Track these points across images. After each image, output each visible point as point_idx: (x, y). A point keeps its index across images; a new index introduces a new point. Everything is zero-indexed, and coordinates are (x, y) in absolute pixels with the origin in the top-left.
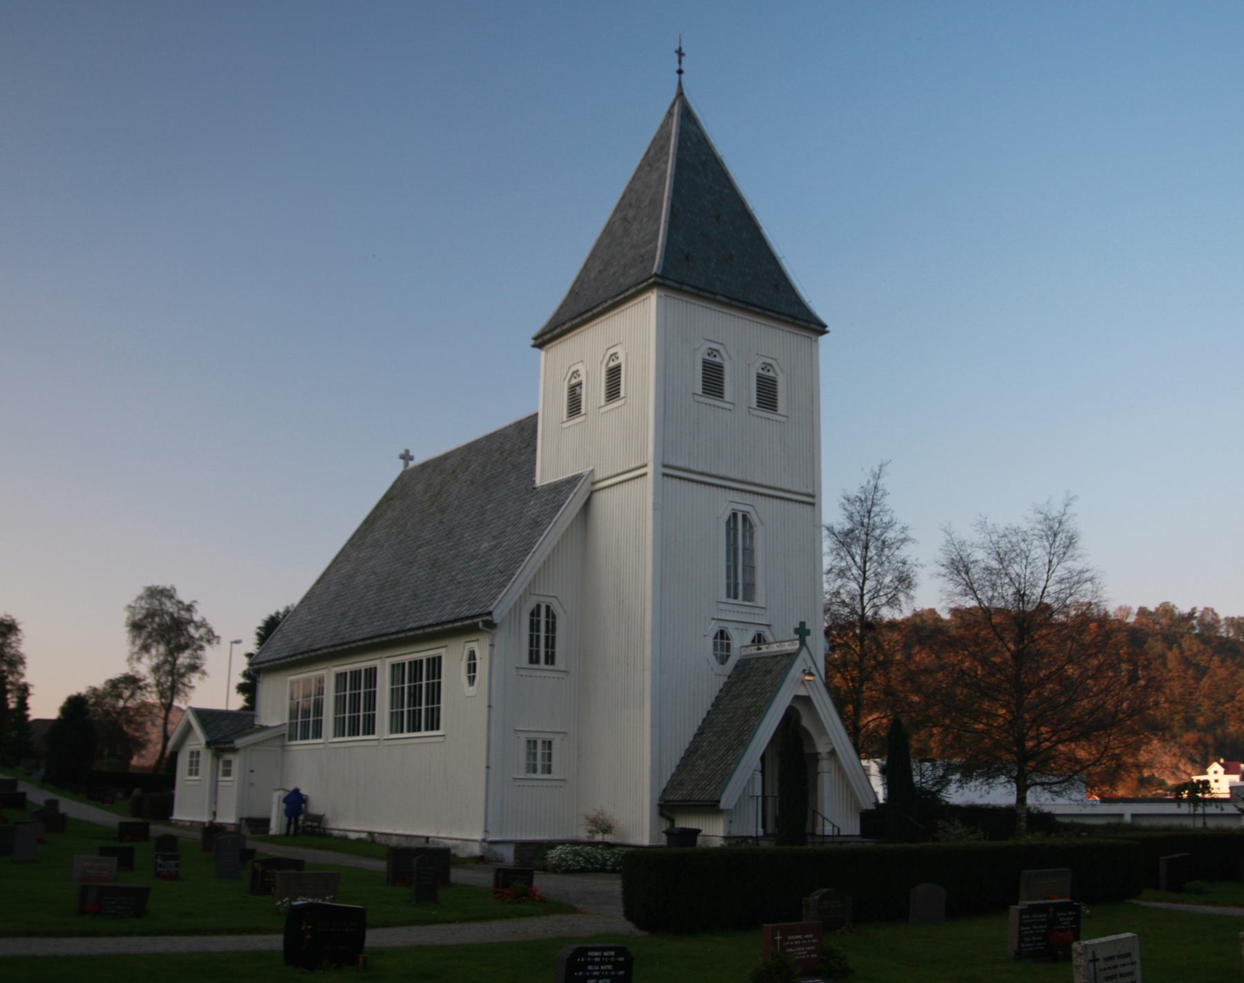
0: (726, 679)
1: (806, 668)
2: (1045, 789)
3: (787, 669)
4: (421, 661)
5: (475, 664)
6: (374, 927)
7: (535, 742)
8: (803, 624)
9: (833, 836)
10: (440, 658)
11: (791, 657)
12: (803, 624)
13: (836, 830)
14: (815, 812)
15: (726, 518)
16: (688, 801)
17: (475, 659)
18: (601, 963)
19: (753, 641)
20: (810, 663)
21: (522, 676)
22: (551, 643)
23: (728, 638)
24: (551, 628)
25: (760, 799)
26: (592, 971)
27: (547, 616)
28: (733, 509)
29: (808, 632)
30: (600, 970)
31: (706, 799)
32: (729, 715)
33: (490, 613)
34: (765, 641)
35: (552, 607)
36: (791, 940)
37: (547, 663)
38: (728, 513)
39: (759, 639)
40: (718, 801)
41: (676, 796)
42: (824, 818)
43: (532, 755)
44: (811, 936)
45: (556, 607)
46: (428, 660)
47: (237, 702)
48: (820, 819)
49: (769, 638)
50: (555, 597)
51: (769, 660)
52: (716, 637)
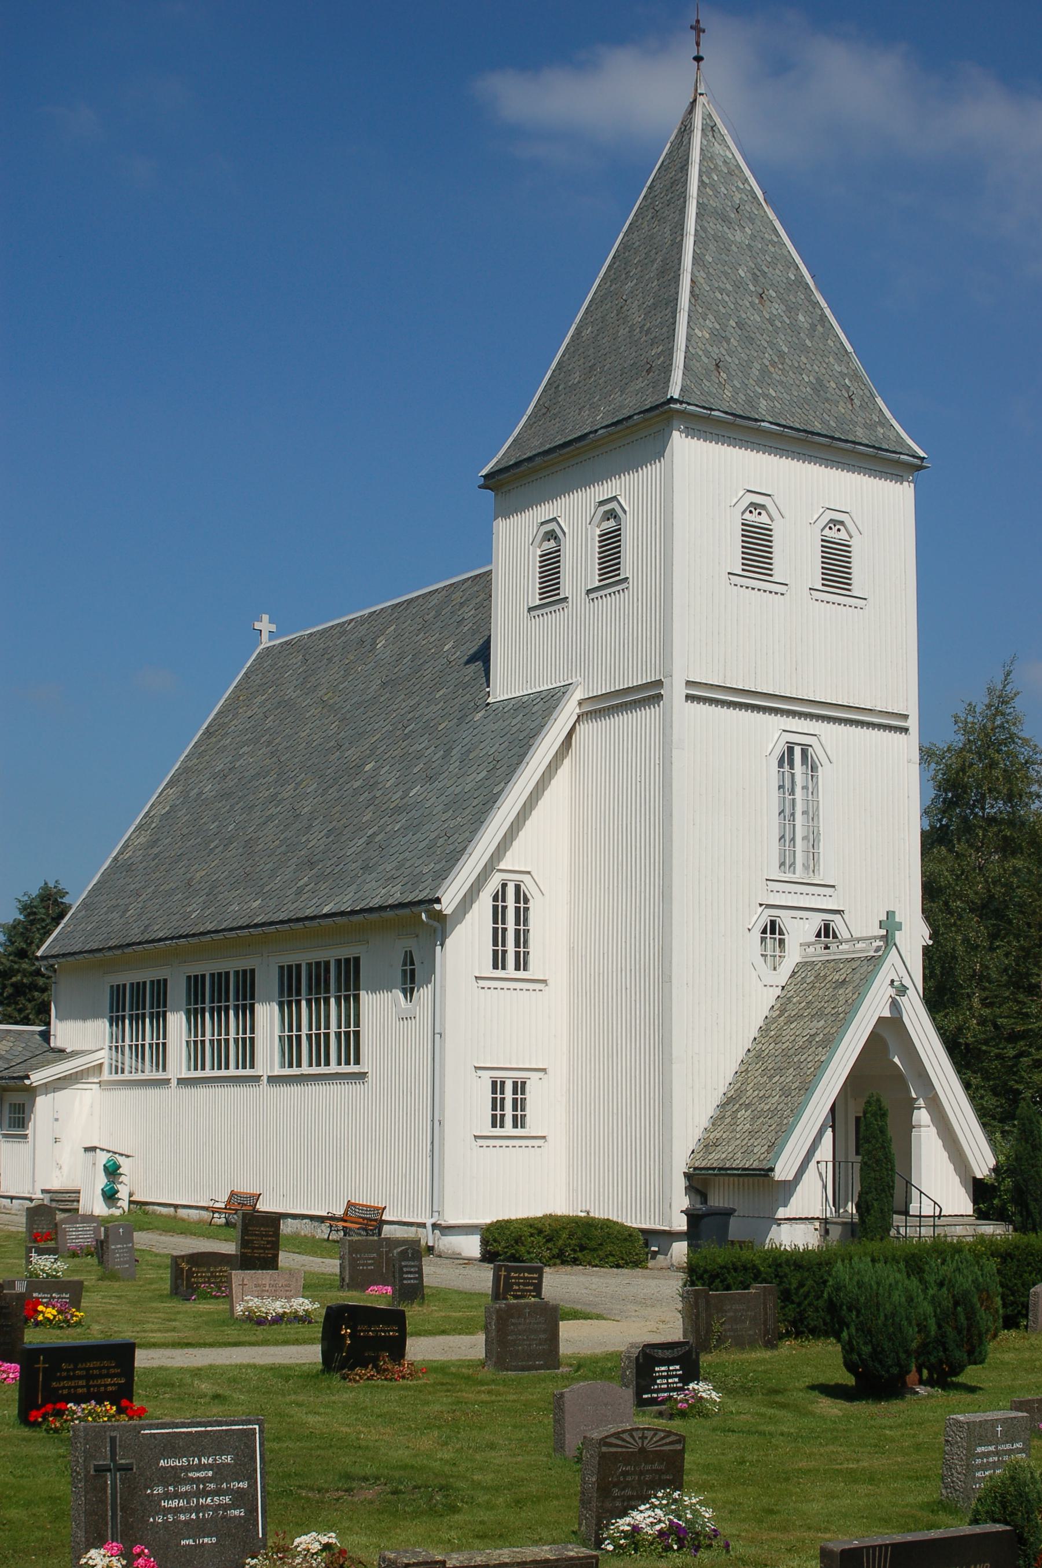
0: (778, 991)
1: (896, 978)
2: (949, 750)
3: (867, 981)
4: (327, 964)
5: (413, 971)
6: (418, 1334)
7: (503, 1083)
8: (890, 914)
9: (934, 1216)
10: (357, 960)
11: (875, 962)
12: (890, 914)
13: (938, 1209)
14: (908, 1183)
15: (777, 753)
16: (728, 1169)
17: (412, 963)
18: (668, 1377)
19: (818, 935)
20: (903, 972)
21: (483, 988)
22: (522, 938)
23: (781, 933)
24: (522, 916)
25: (830, 1165)
26: (661, 1384)
27: (517, 901)
28: (787, 742)
29: (899, 927)
30: (668, 1383)
31: (754, 1166)
32: (785, 1046)
33: (438, 901)
34: (835, 936)
35: (523, 887)
36: (659, 1372)
37: (517, 968)
38: (781, 747)
39: (826, 931)
40: (772, 1170)
41: (714, 1159)
42: (921, 1192)
43: (497, 1104)
44: (678, 1367)
45: (529, 886)
46: (338, 962)
47: (911, 1213)
48: (915, 1193)
49: (843, 933)
50: (529, 873)
51: (842, 966)
52: (764, 932)
